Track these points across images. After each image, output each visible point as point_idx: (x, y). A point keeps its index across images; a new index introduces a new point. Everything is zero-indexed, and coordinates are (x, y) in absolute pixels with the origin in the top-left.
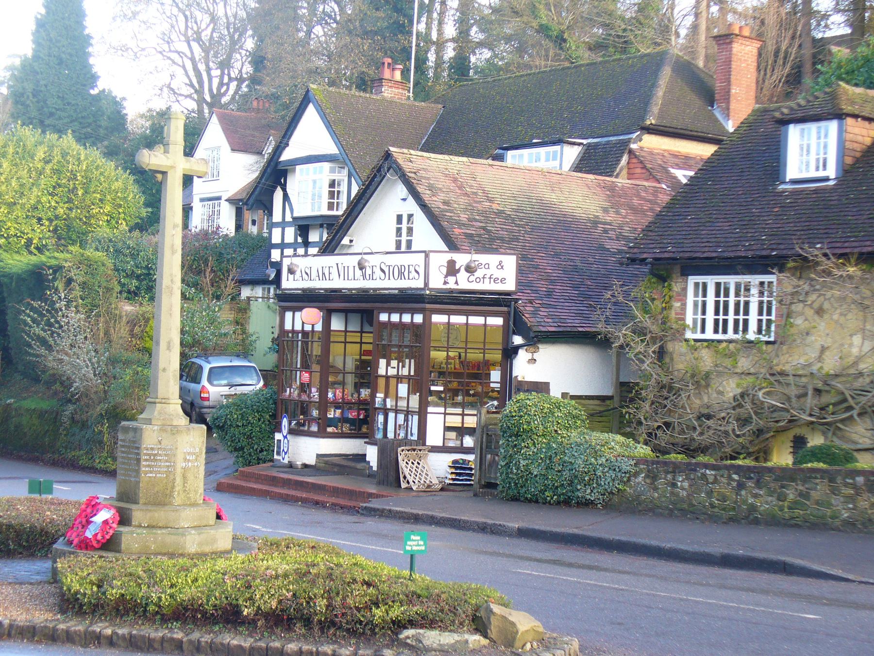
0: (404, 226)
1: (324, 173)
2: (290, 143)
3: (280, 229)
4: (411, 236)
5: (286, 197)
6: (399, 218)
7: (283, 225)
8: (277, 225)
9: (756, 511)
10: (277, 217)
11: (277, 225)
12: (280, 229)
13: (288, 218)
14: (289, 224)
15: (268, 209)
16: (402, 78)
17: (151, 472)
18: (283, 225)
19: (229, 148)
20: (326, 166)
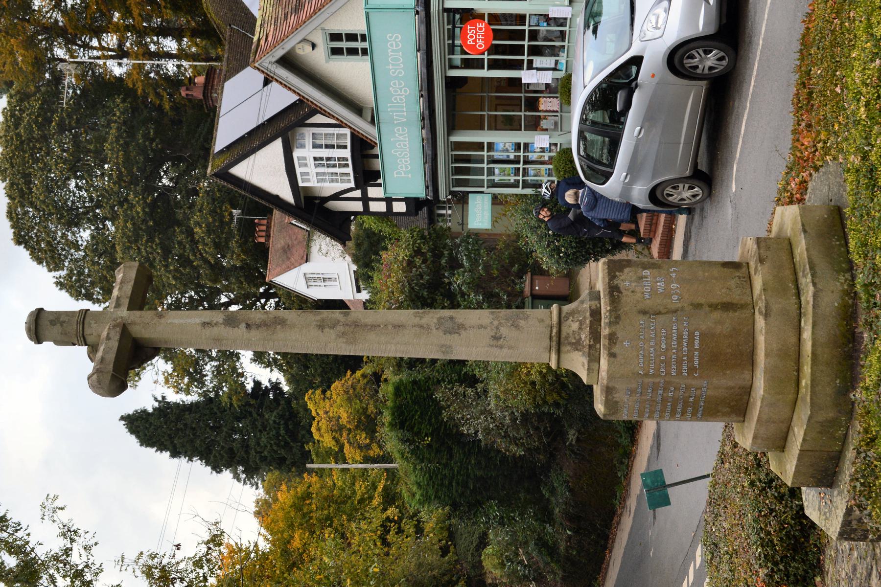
0: (344, 45)
1: (304, 153)
2: (7, 223)
3: (371, 203)
4: (356, 35)
5: (337, 197)
6: (336, 51)
7: (365, 200)
8: (366, 206)
9: (629, 458)
10: (358, 206)
11: (366, 206)
12: (371, 203)
13: (358, 194)
14: (365, 193)
15: (346, 216)
16: (611, 122)
17: (691, 360)
18: (365, 200)
19: (48, 307)
20: (297, 154)
